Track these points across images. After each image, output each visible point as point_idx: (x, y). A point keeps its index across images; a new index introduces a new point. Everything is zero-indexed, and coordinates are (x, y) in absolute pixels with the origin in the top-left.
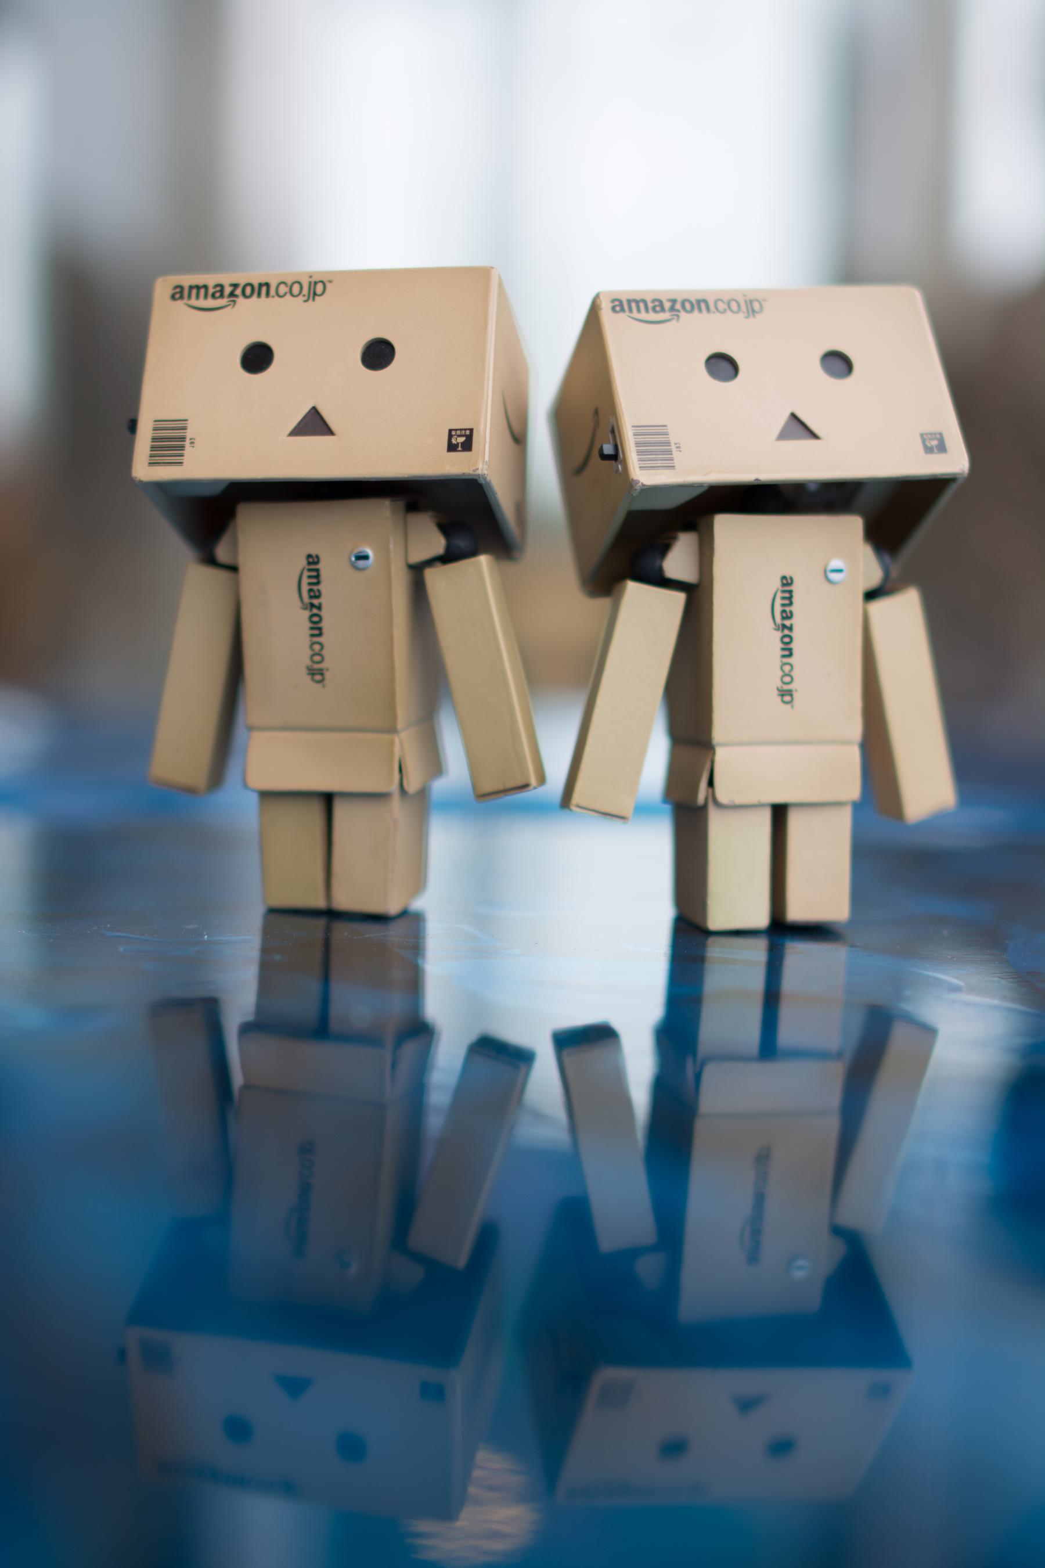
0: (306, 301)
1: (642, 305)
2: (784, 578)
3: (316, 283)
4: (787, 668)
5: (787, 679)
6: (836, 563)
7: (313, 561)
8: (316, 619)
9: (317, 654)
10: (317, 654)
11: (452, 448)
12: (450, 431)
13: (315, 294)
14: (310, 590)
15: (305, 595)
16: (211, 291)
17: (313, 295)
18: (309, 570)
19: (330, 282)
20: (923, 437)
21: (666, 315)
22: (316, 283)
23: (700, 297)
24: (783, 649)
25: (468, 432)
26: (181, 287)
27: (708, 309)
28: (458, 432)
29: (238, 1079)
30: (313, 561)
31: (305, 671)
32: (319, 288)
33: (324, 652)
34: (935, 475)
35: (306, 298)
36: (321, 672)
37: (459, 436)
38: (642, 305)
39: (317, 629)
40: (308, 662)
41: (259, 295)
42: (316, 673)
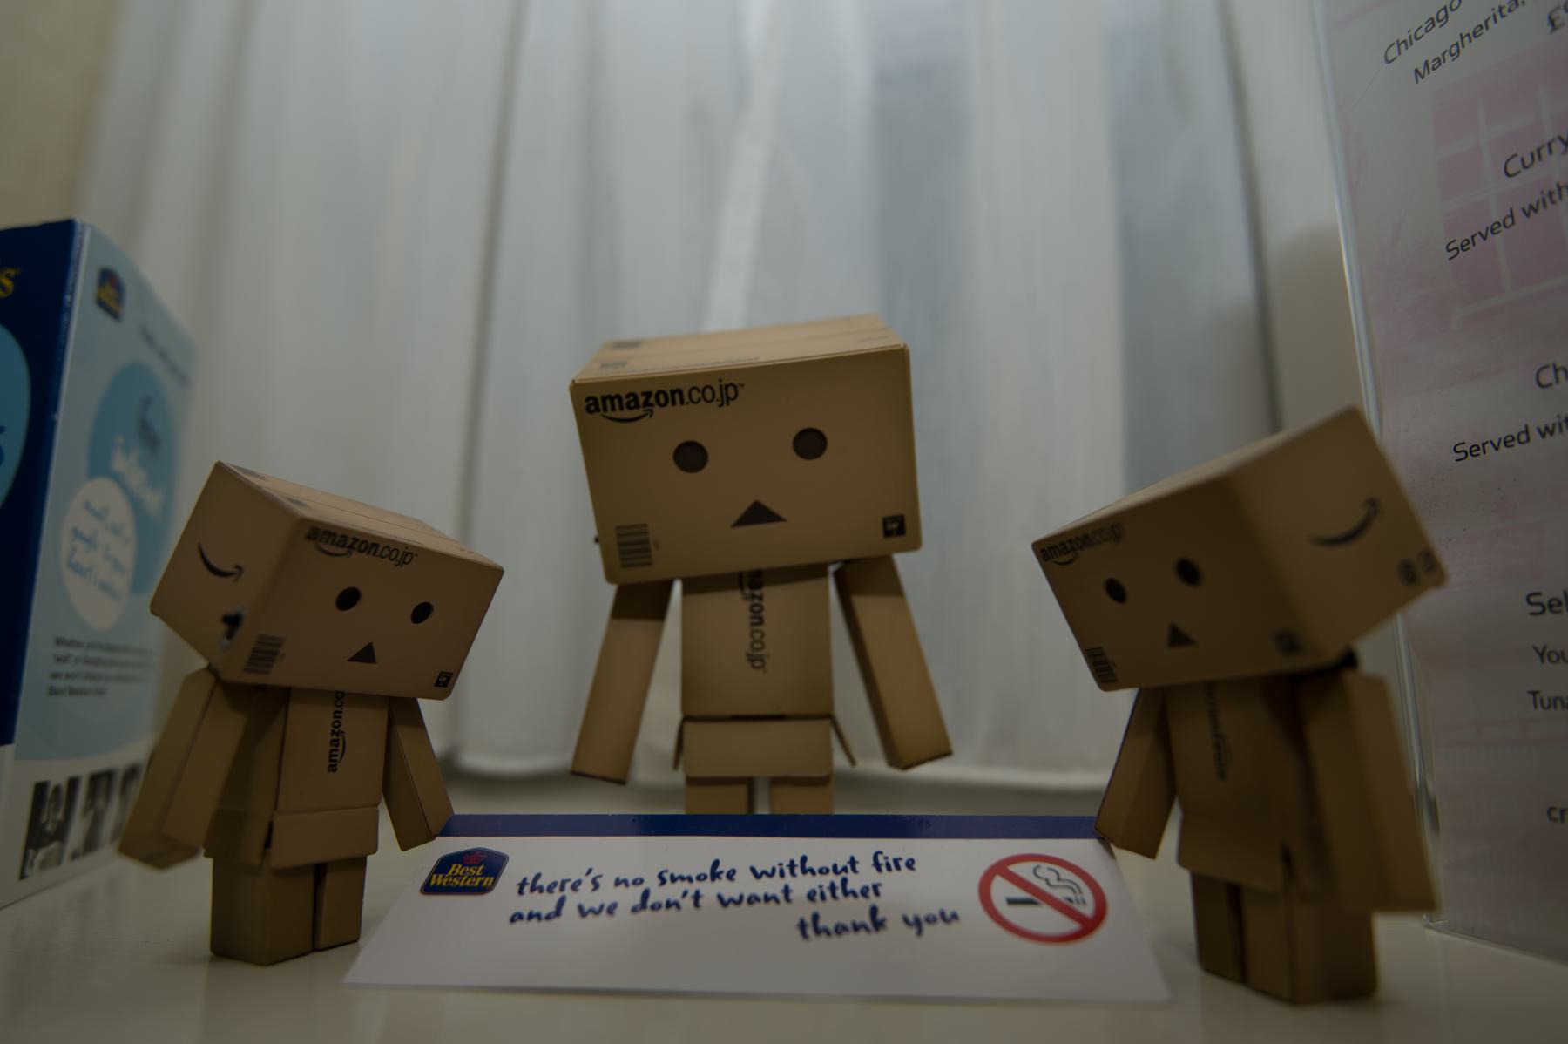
4: (757, 636)
5: (757, 646)
9: (757, 643)
10: (757, 643)
11: (888, 533)
17: (752, 659)
20: (886, 521)
21: (640, 412)
24: (674, 403)
26: (594, 399)
29: (680, 811)
32: (758, 664)
33: (765, 640)
36: (761, 659)
40: (748, 649)
41: (674, 403)
42: (756, 659)
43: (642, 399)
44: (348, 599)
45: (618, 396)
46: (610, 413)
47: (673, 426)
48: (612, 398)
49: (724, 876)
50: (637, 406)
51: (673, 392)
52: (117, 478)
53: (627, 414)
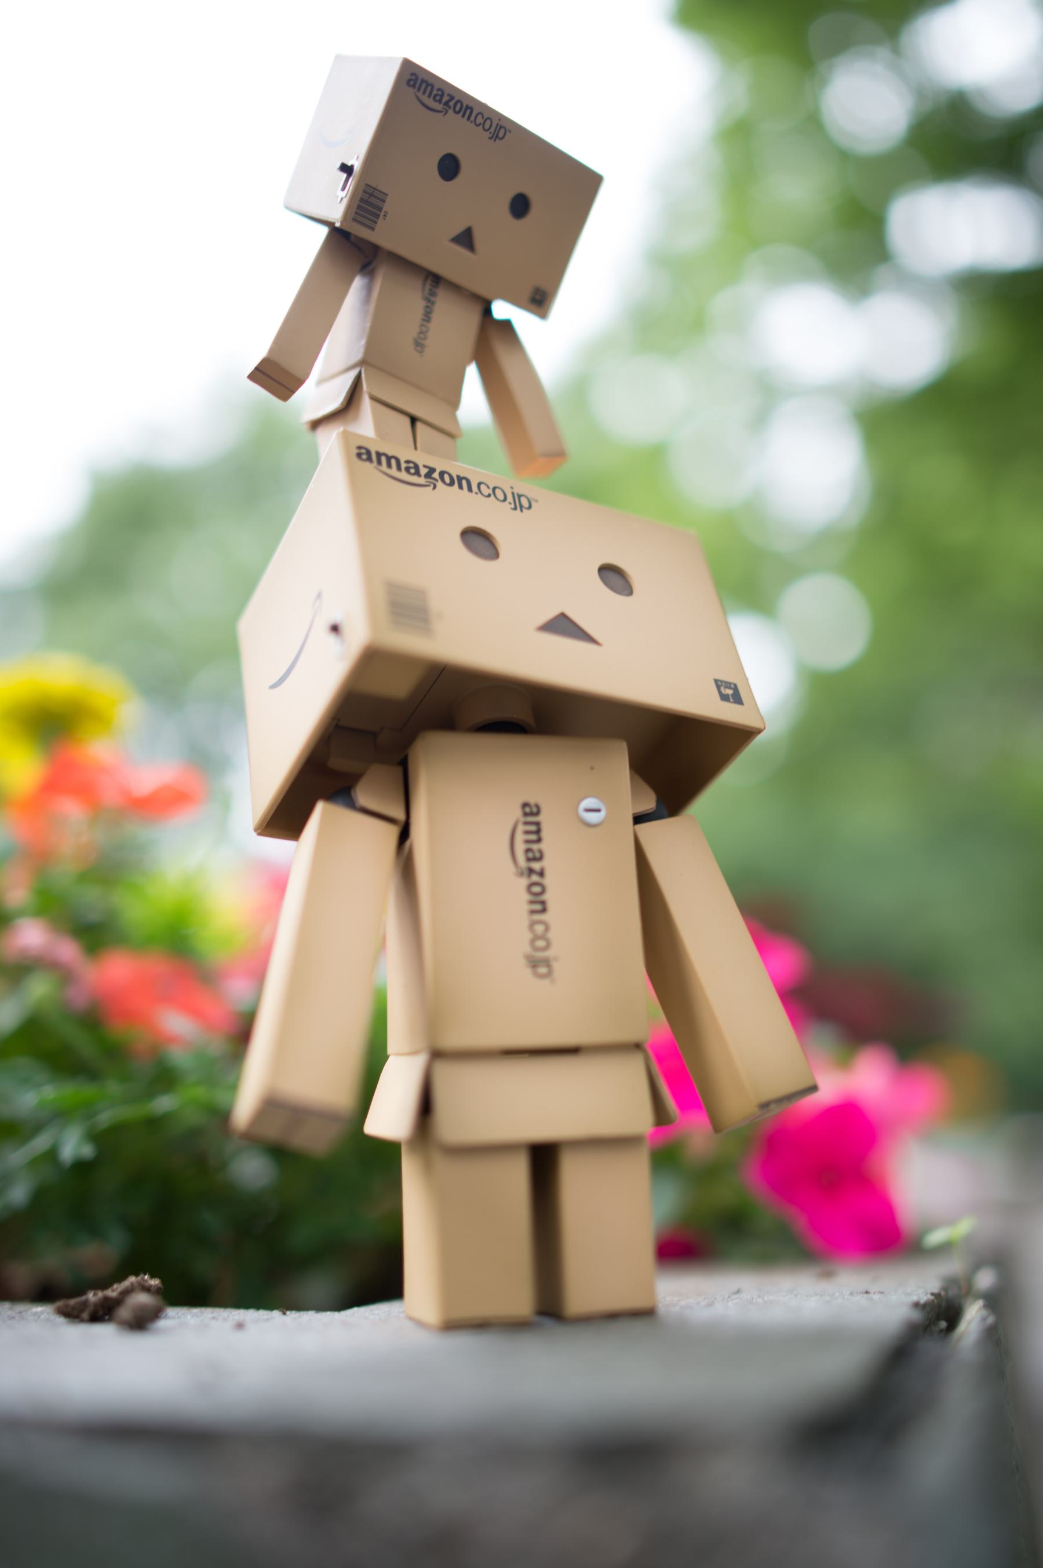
0: (491, 138)
1: (429, 88)
2: (525, 805)
3: (501, 127)
4: (539, 929)
6: (590, 802)
7: (531, 811)
8: (537, 889)
9: (540, 938)
10: (540, 938)
16: (535, 847)
17: (534, 963)
18: (526, 823)
19: (536, 501)
22: (501, 127)
23: (470, 105)
24: (463, 116)
26: (538, 813)
27: (470, 489)
30: (531, 811)
31: (523, 962)
33: (550, 935)
34: (722, 721)
35: (513, 506)
36: (547, 962)
38: (429, 88)
39: (539, 904)
40: (527, 949)
41: (463, 116)
42: (539, 964)
43: (536, 866)
45: (539, 840)
46: (420, 94)
48: (538, 832)
50: (440, 101)
51: (467, 107)
53: (430, 102)
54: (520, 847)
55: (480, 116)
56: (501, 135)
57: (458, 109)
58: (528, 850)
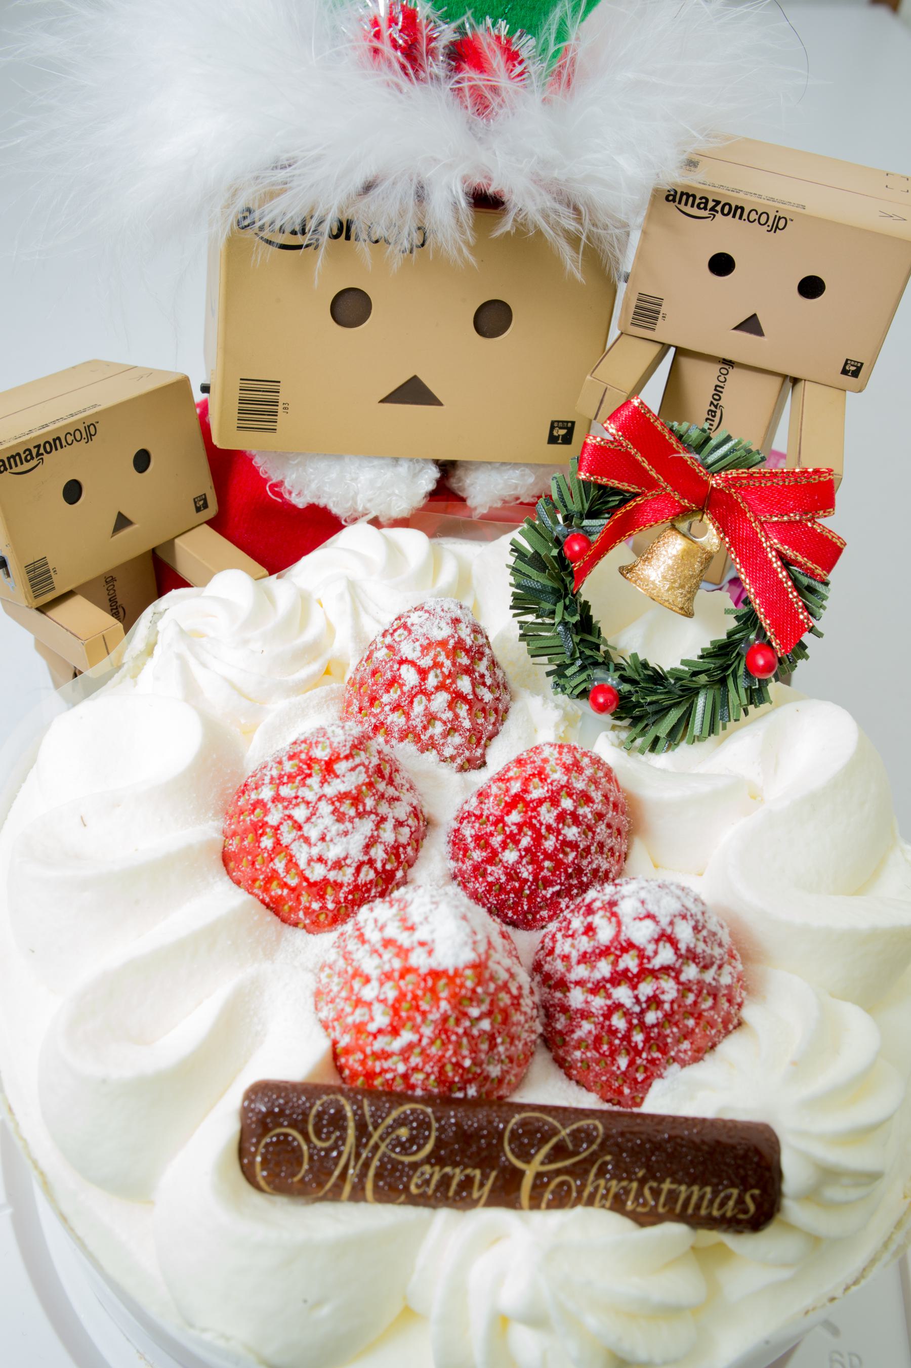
1: (691, 199)
4: (70, 439)
5: (763, 220)
11: (845, 372)
12: (847, 360)
13: (91, 435)
14: (714, 416)
15: (718, 414)
17: (775, 228)
24: (734, 216)
25: (570, 425)
28: (560, 424)
32: (782, 224)
35: (769, 229)
37: (561, 428)
38: (691, 199)
41: (734, 216)
43: (711, 204)
44: (73, 492)
46: (15, 470)
47: (722, 235)
49: (285, 759)
51: (737, 207)
52: (677, 960)
54: (27, 466)
55: (754, 212)
56: (781, 226)
57: (726, 211)
58: (27, 461)
